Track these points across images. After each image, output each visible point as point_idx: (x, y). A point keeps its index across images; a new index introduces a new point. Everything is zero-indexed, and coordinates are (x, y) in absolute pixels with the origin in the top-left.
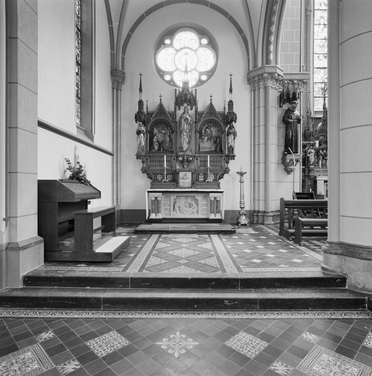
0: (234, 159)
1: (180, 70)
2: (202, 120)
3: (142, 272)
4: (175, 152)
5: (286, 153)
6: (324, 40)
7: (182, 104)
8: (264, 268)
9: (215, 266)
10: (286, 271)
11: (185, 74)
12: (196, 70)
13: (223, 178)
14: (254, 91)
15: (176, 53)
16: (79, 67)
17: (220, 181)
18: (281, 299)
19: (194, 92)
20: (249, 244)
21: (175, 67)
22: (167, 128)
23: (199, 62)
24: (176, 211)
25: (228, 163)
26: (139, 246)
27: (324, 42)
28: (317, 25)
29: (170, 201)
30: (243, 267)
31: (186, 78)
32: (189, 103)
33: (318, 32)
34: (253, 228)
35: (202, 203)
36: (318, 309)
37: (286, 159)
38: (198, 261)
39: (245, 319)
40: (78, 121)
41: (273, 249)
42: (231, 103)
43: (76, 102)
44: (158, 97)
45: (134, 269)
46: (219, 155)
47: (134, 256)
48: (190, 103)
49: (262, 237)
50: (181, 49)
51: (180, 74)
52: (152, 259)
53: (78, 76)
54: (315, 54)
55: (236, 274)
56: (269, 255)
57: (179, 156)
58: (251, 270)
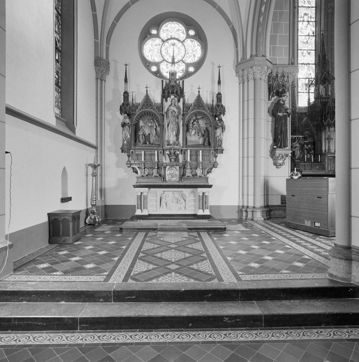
0: (222, 153)
1: (167, 62)
2: (190, 113)
3: (127, 281)
4: (161, 145)
5: (275, 147)
6: (308, 37)
7: (169, 96)
8: (265, 275)
9: (200, 250)
10: (290, 278)
11: (172, 65)
12: (183, 61)
13: (211, 172)
14: (243, 83)
16: (60, 54)
17: (208, 176)
18: (289, 315)
19: (181, 84)
20: (242, 244)
21: (162, 58)
22: (154, 121)
23: (186, 54)
24: (163, 207)
25: (216, 157)
26: (124, 247)
27: (308, 39)
28: (300, 22)
29: (156, 197)
30: (240, 273)
31: (173, 69)
32: (176, 95)
33: (302, 29)
34: (241, 224)
35: (190, 198)
36: (332, 325)
37: (276, 153)
38: (190, 266)
39: (251, 341)
40: (58, 112)
41: (269, 250)
42: (219, 97)
43: (55, 90)
44: (146, 88)
45: (117, 278)
46: (208, 149)
48: (177, 95)
49: (254, 235)
51: (167, 65)
53: (59, 63)
54: (299, 50)
55: (235, 284)
57: (166, 149)
58: (251, 278)
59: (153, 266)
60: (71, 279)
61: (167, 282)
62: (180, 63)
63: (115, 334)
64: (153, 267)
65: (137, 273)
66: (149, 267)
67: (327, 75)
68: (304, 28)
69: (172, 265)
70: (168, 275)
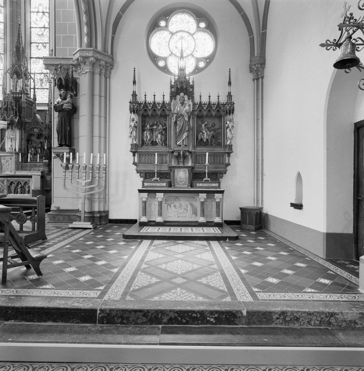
6: (43, 29)
9: (210, 260)
15: (171, 37)
26: (126, 257)
33: (37, 20)
42: (230, 96)
47: (128, 258)
50: (177, 32)
52: (140, 277)
56: (270, 258)
59: (202, 281)
60: (94, 294)
61: (171, 300)
62: (190, 57)
63: (55, 366)
64: (202, 281)
65: (137, 288)
66: (151, 280)
67: (18, 68)
68: (38, 19)
69: (177, 278)
70: (173, 291)
